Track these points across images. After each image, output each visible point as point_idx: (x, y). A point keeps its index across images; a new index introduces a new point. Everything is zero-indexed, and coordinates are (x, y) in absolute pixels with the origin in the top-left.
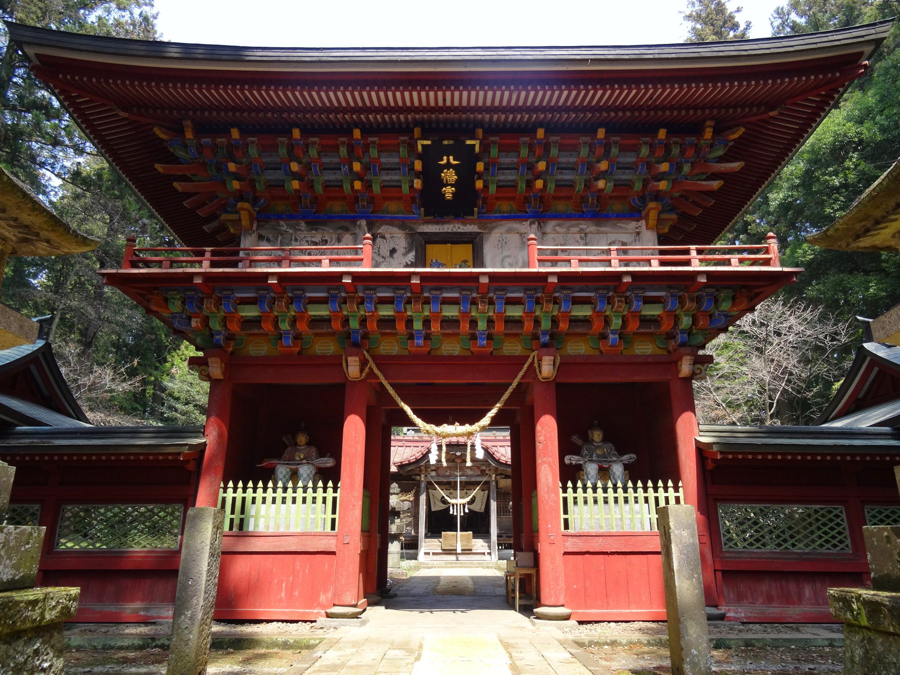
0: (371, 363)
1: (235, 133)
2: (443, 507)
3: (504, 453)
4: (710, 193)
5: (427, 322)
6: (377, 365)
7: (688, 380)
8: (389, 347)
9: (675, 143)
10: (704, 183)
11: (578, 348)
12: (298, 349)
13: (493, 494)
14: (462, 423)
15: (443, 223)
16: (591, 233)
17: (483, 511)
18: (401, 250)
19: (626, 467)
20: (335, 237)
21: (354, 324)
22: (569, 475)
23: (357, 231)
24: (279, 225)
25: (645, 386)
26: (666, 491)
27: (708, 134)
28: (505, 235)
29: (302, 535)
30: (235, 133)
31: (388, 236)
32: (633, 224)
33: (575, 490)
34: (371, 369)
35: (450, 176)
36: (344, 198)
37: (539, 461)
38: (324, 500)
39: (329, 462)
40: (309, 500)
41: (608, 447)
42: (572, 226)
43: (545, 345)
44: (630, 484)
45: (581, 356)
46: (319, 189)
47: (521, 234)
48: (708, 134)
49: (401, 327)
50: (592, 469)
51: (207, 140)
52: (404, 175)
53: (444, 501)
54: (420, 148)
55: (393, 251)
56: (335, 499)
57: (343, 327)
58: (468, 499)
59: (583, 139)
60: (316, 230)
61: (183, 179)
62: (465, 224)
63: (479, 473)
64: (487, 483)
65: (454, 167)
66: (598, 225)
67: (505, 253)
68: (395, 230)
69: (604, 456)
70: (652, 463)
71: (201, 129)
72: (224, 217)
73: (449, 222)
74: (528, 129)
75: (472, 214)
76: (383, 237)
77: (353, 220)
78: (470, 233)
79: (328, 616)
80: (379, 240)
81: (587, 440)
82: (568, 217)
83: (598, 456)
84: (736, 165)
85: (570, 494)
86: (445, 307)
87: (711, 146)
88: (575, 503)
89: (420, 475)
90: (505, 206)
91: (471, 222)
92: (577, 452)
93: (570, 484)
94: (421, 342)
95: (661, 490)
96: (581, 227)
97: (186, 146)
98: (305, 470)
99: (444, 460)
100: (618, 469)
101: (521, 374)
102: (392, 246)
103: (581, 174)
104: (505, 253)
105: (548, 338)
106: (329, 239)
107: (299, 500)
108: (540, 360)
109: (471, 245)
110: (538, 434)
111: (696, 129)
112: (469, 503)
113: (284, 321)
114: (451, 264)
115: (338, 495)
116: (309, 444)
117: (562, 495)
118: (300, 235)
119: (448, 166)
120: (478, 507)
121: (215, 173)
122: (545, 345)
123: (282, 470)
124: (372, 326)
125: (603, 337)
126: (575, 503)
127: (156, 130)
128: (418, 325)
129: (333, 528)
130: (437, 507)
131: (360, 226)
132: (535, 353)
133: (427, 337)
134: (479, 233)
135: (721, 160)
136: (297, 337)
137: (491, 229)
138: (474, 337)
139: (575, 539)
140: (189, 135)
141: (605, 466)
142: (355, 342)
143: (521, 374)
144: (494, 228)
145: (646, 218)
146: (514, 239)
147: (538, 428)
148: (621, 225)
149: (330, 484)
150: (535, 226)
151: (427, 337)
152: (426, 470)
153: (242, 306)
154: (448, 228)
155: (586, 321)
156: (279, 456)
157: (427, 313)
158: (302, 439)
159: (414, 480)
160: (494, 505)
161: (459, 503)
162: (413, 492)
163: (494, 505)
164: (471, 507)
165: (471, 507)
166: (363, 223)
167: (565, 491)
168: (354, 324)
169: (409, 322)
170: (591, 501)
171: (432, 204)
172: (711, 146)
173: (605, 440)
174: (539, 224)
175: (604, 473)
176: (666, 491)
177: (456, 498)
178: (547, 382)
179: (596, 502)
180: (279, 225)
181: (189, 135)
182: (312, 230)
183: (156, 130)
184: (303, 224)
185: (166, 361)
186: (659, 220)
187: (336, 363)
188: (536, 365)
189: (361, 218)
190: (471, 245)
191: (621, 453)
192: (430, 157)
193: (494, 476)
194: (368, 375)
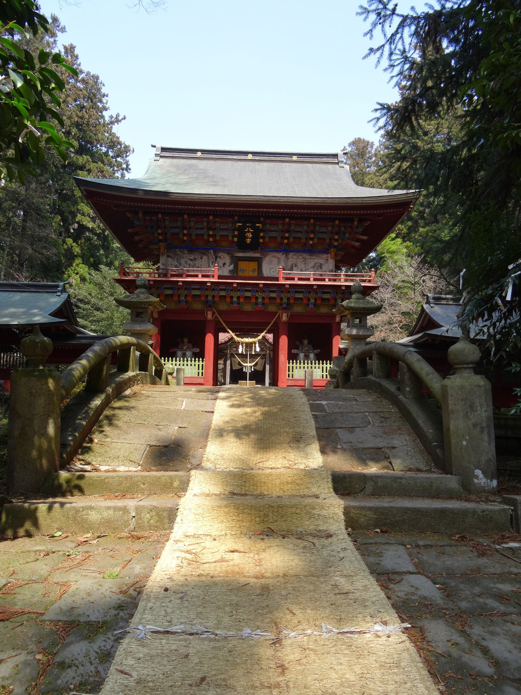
0: (216, 314)
1: (160, 216)
2: (239, 367)
3: (271, 340)
4: (353, 247)
5: (238, 298)
6: (218, 313)
8: (223, 307)
9: (343, 226)
10: (353, 242)
11: (298, 309)
12: (186, 307)
13: (268, 361)
14: (251, 338)
15: (246, 252)
18: (228, 264)
19: (315, 355)
20: (200, 257)
21: (210, 298)
22: (292, 357)
23: (209, 255)
26: (327, 364)
27: (356, 223)
28: (272, 258)
29: (191, 377)
30: (160, 216)
31: (222, 257)
32: (325, 256)
34: (216, 316)
37: (280, 352)
38: (195, 365)
39: (197, 350)
40: (193, 365)
42: (300, 256)
43: (284, 308)
46: (194, 237)
47: (278, 258)
48: (356, 223)
49: (228, 300)
50: (302, 355)
51: (148, 218)
53: (240, 364)
54: (237, 226)
55: (224, 264)
56: (203, 365)
58: (253, 364)
59: (305, 223)
60: (192, 254)
62: (255, 253)
64: (264, 355)
66: (311, 255)
67: (271, 267)
68: (225, 255)
69: (307, 350)
70: (324, 354)
73: (248, 252)
74: (283, 217)
76: (220, 258)
77: (208, 250)
80: (218, 259)
81: (302, 343)
82: (298, 251)
83: (305, 350)
84: (365, 238)
85: (291, 365)
86: (245, 292)
87: (358, 227)
88: (296, 368)
89: (227, 350)
90: (272, 245)
92: (297, 348)
93: (291, 361)
94: (236, 305)
95: (325, 364)
97: (139, 219)
98: (188, 353)
99: (244, 351)
100: (312, 356)
101: (275, 319)
102: (224, 262)
104: (271, 267)
107: (189, 365)
108: (282, 314)
109: (257, 263)
110: (280, 343)
111: (352, 221)
112: (254, 366)
113: (182, 296)
115: (204, 363)
116: (189, 342)
117: (288, 365)
118: (185, 256)
119: (249, 231)
120: (259, 368)
122: (284, 308)
123: (179, 353)
124: (217, 299)
125: (308, 305)
126: (296, 368)
128: (235, 299)
129: (202, 375)
130: (236, 367)
131: (210, 253)
132: (280, 311)
133: (238, 303)
136: (187, 302)
137: (266, 256)
138: (257, 304)
139: (291, 381)
140: (141, 215)
142: (210, 305)
143: (275, 319)
145: (331, 253)
146: (275, 260)
147: (280, 340)
149: (201, 359)
150: (284, 255)
151: (238, 303)
152: (230, 348)
154: (247, 255)
156: (177, 347)
157: (239, 295)
158: (186, 340)
160: (268, 367)
161: (248, 366)
162: (223, 359)
163: (268, 367)
164: (255, 368)
165: (255, 368)
166: (212, 251)
167: (289, 364)
168: (210, 298)
169: (232, 297)
170: (298, 368)
171: (242, 246)
172: (358, 227)
173: (309, 344)
175: (307, 357)
176: (327, 364)
177: (247, 363)
178: (285, 323)
179: (300, 368)
181: (141, 215)
183: (127, 213)
184: (186, 251)
185: (64, 273)
186: (336, 254)
187: (202, 313)
188: (281, 316)
189: (211, 249)
190: (257, 263)
192: (241, 230)
194: (215, 318)
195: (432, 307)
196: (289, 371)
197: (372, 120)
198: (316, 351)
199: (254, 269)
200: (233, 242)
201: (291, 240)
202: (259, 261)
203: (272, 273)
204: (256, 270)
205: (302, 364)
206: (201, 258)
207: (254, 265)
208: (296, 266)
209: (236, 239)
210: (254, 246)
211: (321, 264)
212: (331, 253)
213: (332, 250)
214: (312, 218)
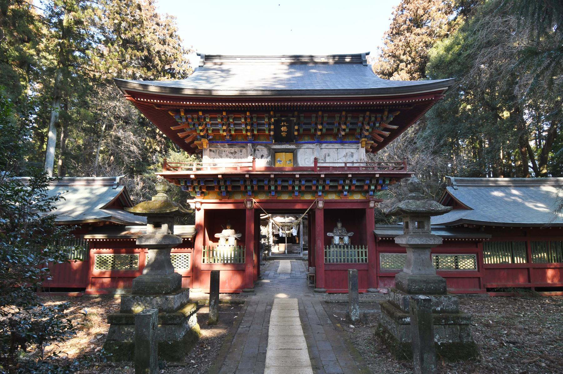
11: (333, 197)
15: (282, 144)
18: (265, 156)
20: (239, 150)
30: (200, 113)
32: (357, 145)
41: (344, 230)
48: (386, 113)
59: (336, 115)
60: (232, 147)
61: (182, 130)
62: (290, 145)
68: (263, 147)
73: (284, 144)
79: (244, 292)
80: (257, 151)
84: (395, 127)
91: (293, 144)
97: (181, 117)
114: (284, 162)
119: (284, 126)
127: (170, 112)
134: (295, 149)
135: (391, 123)
158: (339, 225)
167: (326, 249)
171: (279, 139)
173: (342, 226)
181: (182, 114)
183: (170, 112)
184: (226, 145)
189: (249, 143)
191: (348, 231)
195: (455, 189)
196: (326, 256)
197: (284, 57)
198: (350, 234)
199: (290, 160)
200: (270, 135)
201: (301, 131)
202: (294, 152)
203: (307, 163)
204: (292, 161)
205: (364, 259)
206: (241, 151)
207: (290, 156)
208: (329, 156)
209: (272, 133)
210: (289, 139)
211: (352, 153)
212: (361, 143)
213: (363, 139)
214: (344, 110)
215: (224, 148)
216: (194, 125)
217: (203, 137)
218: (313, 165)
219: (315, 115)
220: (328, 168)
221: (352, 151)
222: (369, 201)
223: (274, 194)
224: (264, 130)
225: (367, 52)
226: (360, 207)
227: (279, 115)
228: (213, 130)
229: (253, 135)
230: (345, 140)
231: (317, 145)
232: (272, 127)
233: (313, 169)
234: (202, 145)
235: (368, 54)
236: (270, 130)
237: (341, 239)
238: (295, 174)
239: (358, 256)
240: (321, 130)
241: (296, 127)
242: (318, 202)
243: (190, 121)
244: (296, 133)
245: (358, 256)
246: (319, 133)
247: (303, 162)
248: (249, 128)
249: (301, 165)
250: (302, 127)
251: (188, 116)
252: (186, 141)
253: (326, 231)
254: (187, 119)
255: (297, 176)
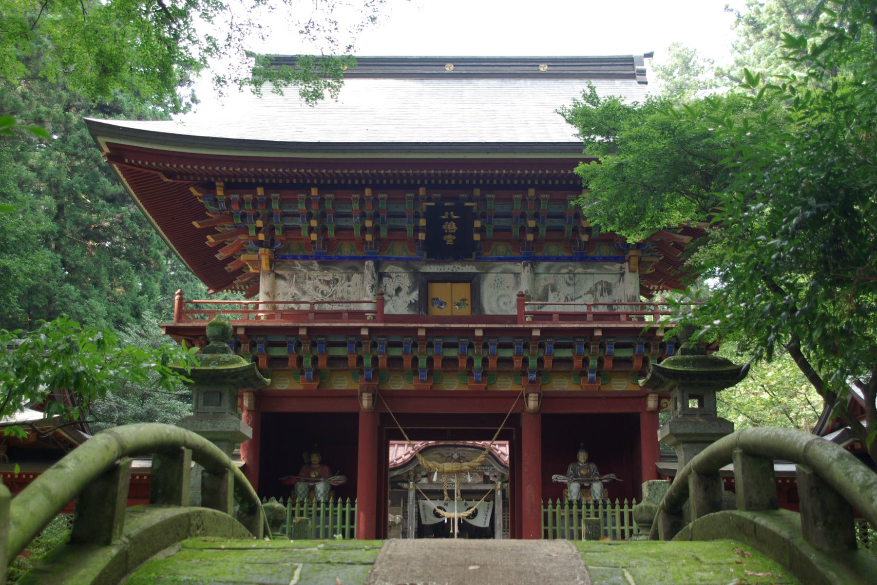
7: (654, 413)
11: (563, 385)
16: (579, 273)
17: (487, 525)
18: (405, 289)
20: (344, 275)
24: (294, 265)
25: (628, 415)
31: (394, 275)
33: (554, 506)
35: (452, 227)
36: (354, 240)
44: (608, 501)
45: (565, 392)
52: (410, 222)
55: (398, 290)
57: (358, 365)
60: (328, 269)
63: (481, 479)
65: (454, 220)
68: (400, 269)
71: (229, 187)
72: (243, 257)
73: (449, 263)
75: (471, 257)
78: (469, 273)
80: (385, 279)
89: (408, 482)
91: (470, 263)
96: (570, 268)
97: (216, 200)
102: (397, 285)
103: (570, 223)
105: (535, 376)
106: (340, 279)
109: (469, 285)
114: (450, 300)
117: (543, 510)
118: (313, 274)
119: (450, 219)
121: (240, 222)
127: (192, 190)
140: (220, 193)
141: (586, 485)
144: (493, 267)
146: (509, 279)
148: (607, 267)
150: (528, 268)
153: (272, 348)
154: (448, 268)
155: (569, 360)
158: (582, 457)
159: (401, 488)
167: (546, 507)
171: (436, 249)
174: (532, 265)
178: (534, 413)
180: (294, 265)
181: (220, 193)
182: (324, 269)
183: (192, 190)
184: (316, 264)
187: (354, 396)
191: (602, 472)
193: (500, 483)
196: (546, 524)
202: (474, 282)
203: (504, 307)
204: (468, 302)
206: (349, 279)
207: (462, 290)
208: (554, 290)
209: (422, 236)
210: (463, 249)
212: (628, 261)
215: (310, 270)
216: (243, 216)
217: (260, 244)
218: (515, 312)
219: (520, 196)
220: (548, 316)
221: (608, 278)
222: (647, 395)
223: (425, 378)
224: (351, 229)
225: (648, 51)
226: (626, 409)
227: (438, 195)
228: (286, 229)
229: (378, 239)
230: (592, 254)
231: (525, 265)
232: (423, 222)
233: (513, 319)
234: (257, 263)
235: (650, 55)
236: (417, 230)
237: (585, 489)
238: (473, 330)
239: (622, 524)
240: (535, 230)
241: (477, 224)
242: (527, 396)
243: (235, 207)
244: (477, 237)
245: (622, 524)
246: (530, 237)
247: (494, 305)
248: (314, 223)
249: (488, 312)
250: (490, 223)
251: (232, 197)
252: (217, 256)
253: (546, 474)
254: (229, 203)
255: (479, 333)
